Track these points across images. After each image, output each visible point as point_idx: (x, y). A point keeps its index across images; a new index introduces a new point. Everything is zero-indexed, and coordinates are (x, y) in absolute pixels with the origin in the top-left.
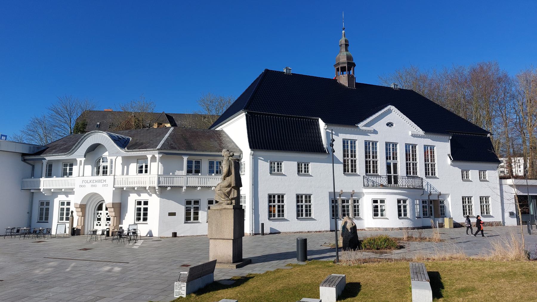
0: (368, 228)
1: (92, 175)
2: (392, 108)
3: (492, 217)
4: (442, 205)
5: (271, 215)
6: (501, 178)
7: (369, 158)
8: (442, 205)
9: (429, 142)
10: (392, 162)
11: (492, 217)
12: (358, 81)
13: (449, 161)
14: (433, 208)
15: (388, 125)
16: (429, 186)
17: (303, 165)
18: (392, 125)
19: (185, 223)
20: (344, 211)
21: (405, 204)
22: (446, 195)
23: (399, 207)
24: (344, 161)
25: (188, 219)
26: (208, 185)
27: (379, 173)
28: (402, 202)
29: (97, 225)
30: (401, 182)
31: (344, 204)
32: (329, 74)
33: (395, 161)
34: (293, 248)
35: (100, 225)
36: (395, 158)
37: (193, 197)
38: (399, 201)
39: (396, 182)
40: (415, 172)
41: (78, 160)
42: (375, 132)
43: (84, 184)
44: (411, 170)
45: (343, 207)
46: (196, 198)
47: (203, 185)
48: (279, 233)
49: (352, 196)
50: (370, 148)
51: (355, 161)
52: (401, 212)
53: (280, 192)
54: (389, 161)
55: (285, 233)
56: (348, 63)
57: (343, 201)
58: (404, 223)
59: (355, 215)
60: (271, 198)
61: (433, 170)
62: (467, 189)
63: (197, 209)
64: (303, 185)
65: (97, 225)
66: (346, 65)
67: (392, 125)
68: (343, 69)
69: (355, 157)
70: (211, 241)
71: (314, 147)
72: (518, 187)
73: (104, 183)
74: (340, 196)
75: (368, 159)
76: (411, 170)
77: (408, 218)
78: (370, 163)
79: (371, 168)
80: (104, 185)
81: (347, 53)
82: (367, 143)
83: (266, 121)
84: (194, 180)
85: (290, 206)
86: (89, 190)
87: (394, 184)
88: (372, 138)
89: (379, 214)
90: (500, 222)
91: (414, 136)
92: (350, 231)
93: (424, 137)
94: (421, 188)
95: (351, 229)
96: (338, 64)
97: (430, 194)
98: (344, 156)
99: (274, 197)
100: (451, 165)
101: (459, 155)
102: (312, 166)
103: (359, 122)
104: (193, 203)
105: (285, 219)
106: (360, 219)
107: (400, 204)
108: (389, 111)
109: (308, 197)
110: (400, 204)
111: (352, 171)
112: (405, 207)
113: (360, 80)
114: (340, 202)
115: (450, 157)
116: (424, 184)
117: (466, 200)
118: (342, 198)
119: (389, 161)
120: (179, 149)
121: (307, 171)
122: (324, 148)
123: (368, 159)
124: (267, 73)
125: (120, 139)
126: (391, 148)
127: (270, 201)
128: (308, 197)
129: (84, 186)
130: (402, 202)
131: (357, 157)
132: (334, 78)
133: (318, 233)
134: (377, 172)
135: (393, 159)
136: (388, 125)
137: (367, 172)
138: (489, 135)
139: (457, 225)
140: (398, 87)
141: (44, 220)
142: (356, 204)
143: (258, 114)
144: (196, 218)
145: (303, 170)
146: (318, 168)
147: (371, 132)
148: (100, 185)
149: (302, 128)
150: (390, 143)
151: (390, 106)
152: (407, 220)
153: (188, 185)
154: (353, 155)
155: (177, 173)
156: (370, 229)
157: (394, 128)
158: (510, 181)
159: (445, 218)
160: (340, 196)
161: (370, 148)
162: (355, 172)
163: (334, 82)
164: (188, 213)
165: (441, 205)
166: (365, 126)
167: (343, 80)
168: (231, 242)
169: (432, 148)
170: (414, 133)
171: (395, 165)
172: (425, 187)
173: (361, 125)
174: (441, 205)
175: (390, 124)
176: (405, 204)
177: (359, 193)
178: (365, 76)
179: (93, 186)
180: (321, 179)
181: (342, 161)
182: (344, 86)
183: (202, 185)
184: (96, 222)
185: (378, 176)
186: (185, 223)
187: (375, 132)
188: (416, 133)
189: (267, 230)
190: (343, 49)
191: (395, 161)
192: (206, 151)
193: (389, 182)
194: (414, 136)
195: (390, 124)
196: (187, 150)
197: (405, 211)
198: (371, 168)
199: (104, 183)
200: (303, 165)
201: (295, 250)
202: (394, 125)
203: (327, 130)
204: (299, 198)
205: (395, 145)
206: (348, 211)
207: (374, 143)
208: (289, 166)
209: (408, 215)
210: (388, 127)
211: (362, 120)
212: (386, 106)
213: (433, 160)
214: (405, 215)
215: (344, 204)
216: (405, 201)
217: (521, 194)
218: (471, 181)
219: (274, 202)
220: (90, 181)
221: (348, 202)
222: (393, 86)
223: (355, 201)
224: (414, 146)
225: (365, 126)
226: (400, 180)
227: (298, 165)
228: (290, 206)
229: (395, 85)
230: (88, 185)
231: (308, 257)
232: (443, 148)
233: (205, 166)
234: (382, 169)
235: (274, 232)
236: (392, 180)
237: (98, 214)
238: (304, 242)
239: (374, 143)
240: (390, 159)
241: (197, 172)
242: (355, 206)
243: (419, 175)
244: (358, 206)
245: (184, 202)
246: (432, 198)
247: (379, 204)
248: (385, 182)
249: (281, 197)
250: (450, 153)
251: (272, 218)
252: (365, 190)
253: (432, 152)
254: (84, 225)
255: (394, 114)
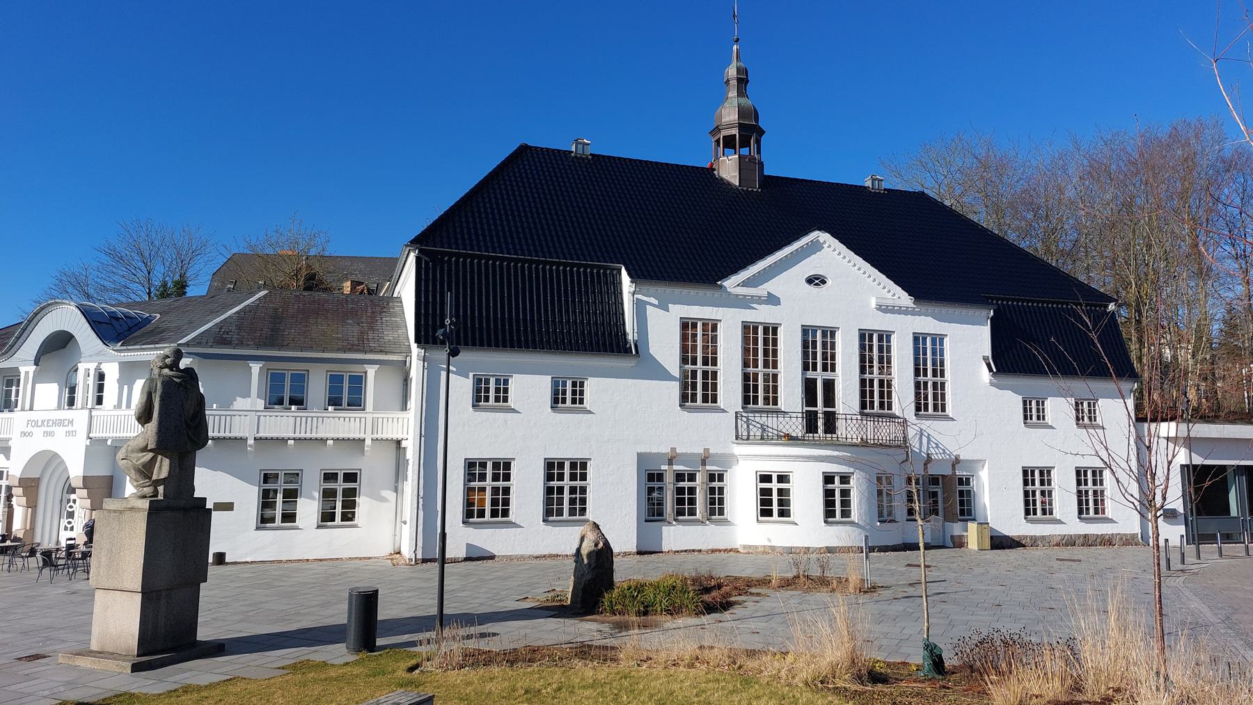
0: (745, 547)
1: (59, 407)
2: (824, 237)
3: (1059, 522)
4: (964, 488)
5: (471, 512)
6: (1140, 419)
7: (925, 375)
8: (964, 488)
9: (927, 324)
10: (819, 376)
11: (1059, 522)
12: (768, 172)
13: (985, 375)
14: (947, 494)
15: (810, 281)
16: (925, 440)
17: (1034, 403)
18: (824, 282)
19: (257, 528)
20: (680, 502)
21: (845, 486)
22: (974, 464)
23: (829, 494)
24: (684, 374)
25: (265, 521)
26: (319, 435)
27: (782, 405)
28: (837, 479)
29: (66, 529)
30: (848, 429)
31: (681, 484)
32: (696, 159)
33: (828, 375)
34: (339, 613)
35: (72, 529)
36: (830, 365)
37: (278, 463)
38: (828, 479)
39: (830, 427)
40: (886, 403)
41: (23, 370)
42: (772, 300)
43: (30, 429)
44: (874, 397)
45: (680, 491)
46: (292, 466)
47: (303, 435)
48: (492, 557)
49: (704, 463)
50: (762, 343)
51: (943, 384)
52: (834, 504)
53: (501, 454)
54: (810, 374)
55: (510, 558)
56: (741, 127)
57: (680, 477)
58: (836, 536)
59: (712, 513)
60: (474, 468)
61: (940, 397)
62: (1036, 448)
63: (291, 495)
64: (565, 436)
65: (66, 529)
66: (735, 131)
67: (824, 282)
68: (729, 142)
69: (942, 375)
70: (98, 594)
71: (609, 340)
72: (1190, 443)
73: (70, 428)
74: (670, 462)
75: (921, 378)
76: (874, 397)
77: (852, 523)
78: (872, 385)
79: (757, 393)
80: (68, 433)
81: (743, 101)
82: (748, 329)
83: (472, 272)
84: (282, 423)
85: (527, 491)
86: (39, 443)
87: (826, 432)
88: (763, 314)
89: (774, 507)
90: (1134, 536)
91: (884, 309)
92: (586, 561)
93: (913, 313)
94: (904, 445)
95: (589, 555)
96: (717, 130)
97: (929, 459)
98: (684, 360)
99: (561, 465)
100: (992, 384)
101: (1009, 359)
102: (592, 387)
103: (725, 275)
104: (340, 477)
105: (510, 523)
106: (726, 522)
107: (830, 486)
108: (816, 247)
109: (579, 468)
110: (830, 486)
111: (935, 409)
112: (845, 493)
113: (775, 167)
114: (669, 479)
115: (989, 365)
116: (911, 433)
117: (1035, 481)
118: (675, 467)
119: (810, 374)
120: (241, 344)
121: (578, 397)
122: (626, 341)
123: (921, 378)
124: (524, 150)
125: (117, 319)
126: (817, 346)
127: (549, 477)
128: (579, 468)
129: (30, 434)
130: (837, 479)
131: (781, 365)
132: (707, 166)
133: (549, 562)
134: (890, 408)
135: (825, 369)
136: (810, 281)
137: (746, 400)
138: (1112, 307)
139: (1000, 543)
140: (885, 185)
141: (566, 515)
142: (716, 484)
143: (451, 255)
144: (289, 517)
145: (566, 396)
146: (606, 389)
147: (759, 300)
148: (60, 431)
149: (580, 291)
150: (814, 329)
151: (827, 236)
152: (848, 528)
153: (262, 434)
154: (711, 359)
155: (240, 403)
156: (751, 550)
157: (829, 289)
158: (1167, 429)
159: (969, 524)
160: (670, 462)
161: (762, 343)
162: (943, 410)
163: (707, 175)
164: (267, 501)
165: (961, 488)
166: (745, 284)
167: (728, 169)
168: (138, 598)
169: (938, 340)
170: (884, 302)
171: (829, 386)
172: (914, 443)
173: (732, 283)
174: (961, 488)
175: (816, 280)
176: (845, 486)
177: (723, 455)
178: (781, 161)
179: (47, 434)
180: (624, 420)
181: (676, 372)
182: (729, 184)
183: (297, 435)
184: (64, 522)
185: (778, 412)
186: (257, 528)
187: (772, 300)
188: (890, 303)
189: (455, 550)
190: (733, 93)
191: (828, 375)
192: (311, 349)
193: (811, 427)
194: (884, 309)
195: (816, 280)
196: (258, 347)
197: (846, 503)
198: (757, 393)
199: (70, 428)
200: (1034, 403)
201: (342, 619)
202: (829, 282)
203: (640, 297)
204: (552, 468)
205: (829, 333)
206: (692, 502)
207: (771, 331)
208: (530, 385)
209: (855, 516)
210: (811, 288)
211: (735, 270)
212: (806, 233)
213: (939, 371)
214: (846, 514)
215: (681, 484)
216: (845, 479)
217: (1198, 460)
218: (1051, 427)
219: (561, 477)
220: (43, 422)
221: (692, 477)
222: (868, 184)
223: (712, 477)
224: (885, 337)
225: (745, 284)
226: (840, 424)
227: (1025, 402)
228: (527, 491)
229: (873, 180)
230: (38, 432)
231: (380, 642)
232: (968, 341)
233: (317, 387)
234: (790, 395)
235: (476, 556)
236: (819, 421)
237: (69, 501)
238: (367, 602)
239: (771, 331)
240: (815, 369)
241: (356, 403)
242: (712, 490)
243: (896, 410)
244: (721, 490)
245: (259, 477)
246: (933, 470)
247: (775, 486)
248: (796, 427)
249: (503, 469)
250: (988, 353)
251: (475, 519)
252: (739, 450)
253: (938, 352)
254: (33, 528)
255: (830, 254)
